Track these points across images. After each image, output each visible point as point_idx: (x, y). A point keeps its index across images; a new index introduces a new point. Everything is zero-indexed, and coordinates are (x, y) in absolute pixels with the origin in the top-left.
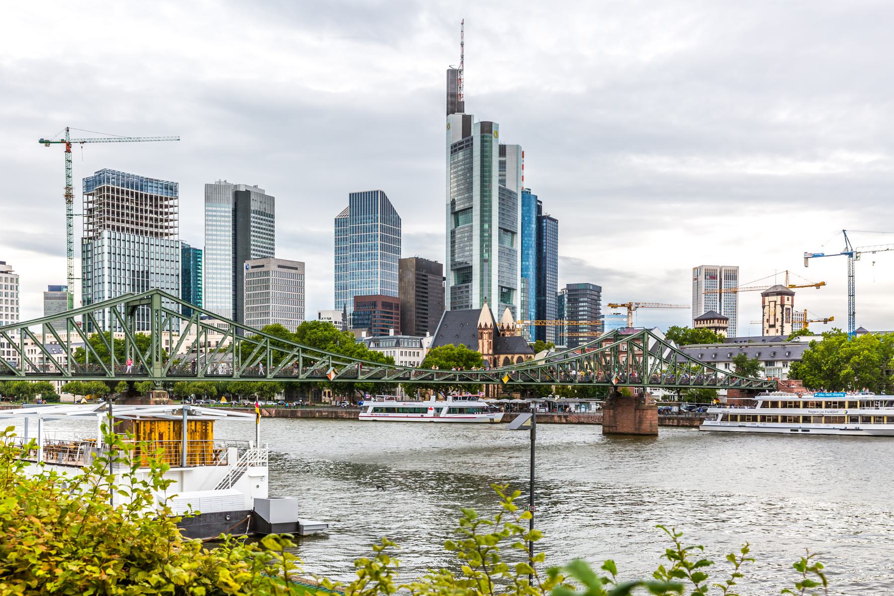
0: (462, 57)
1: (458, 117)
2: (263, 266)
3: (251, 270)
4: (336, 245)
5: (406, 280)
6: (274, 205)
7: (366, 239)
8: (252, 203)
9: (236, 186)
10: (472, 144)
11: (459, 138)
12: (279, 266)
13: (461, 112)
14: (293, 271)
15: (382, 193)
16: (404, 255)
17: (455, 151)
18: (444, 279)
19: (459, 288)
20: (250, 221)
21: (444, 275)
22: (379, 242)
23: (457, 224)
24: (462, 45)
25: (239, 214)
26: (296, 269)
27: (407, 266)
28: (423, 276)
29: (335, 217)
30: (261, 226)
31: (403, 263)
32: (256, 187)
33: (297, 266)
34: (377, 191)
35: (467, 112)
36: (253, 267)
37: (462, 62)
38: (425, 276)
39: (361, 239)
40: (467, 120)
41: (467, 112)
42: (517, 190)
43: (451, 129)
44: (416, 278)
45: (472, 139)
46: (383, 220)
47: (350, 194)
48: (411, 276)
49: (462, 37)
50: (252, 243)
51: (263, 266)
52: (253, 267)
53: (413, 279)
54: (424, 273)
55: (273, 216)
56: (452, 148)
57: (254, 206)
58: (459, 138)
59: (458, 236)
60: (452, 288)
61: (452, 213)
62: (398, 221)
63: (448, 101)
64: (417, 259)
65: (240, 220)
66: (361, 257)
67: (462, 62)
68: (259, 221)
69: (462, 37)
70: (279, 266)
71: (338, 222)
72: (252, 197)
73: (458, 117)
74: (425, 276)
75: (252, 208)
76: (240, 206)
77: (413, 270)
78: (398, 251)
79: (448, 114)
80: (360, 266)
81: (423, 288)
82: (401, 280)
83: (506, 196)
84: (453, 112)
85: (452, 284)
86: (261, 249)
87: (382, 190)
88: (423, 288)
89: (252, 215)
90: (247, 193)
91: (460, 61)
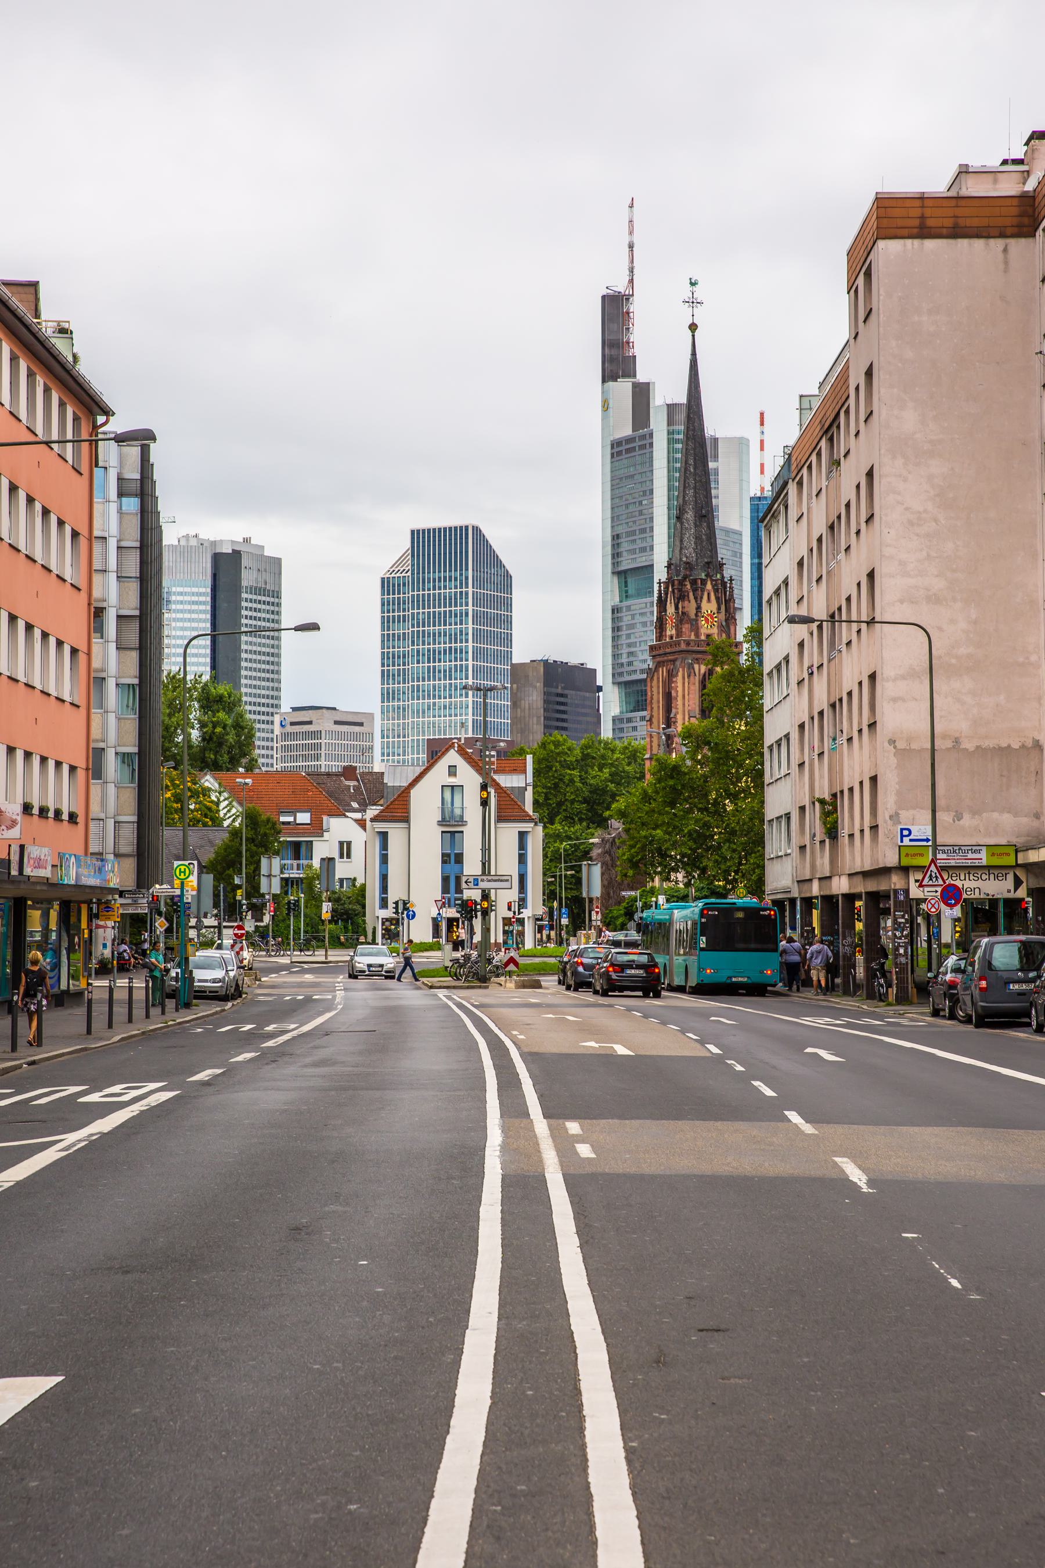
0: (631, 270)
1: (623, 388)
2: (310, 723)
3: (290, 729)
4: (383, 630)
5: (525, 704)
6: (280, 573)
7: (442, 618)
8: (244, 574)
9: (214, 543)
10: (651, 445)
11: (627, 431)
12: (336, 723)
13: (629, 376)
14: (357, 729)
15: (477, 530)
16: (521, 654)
17: (619, 453)
18: (600, 689)
19: (629, 720)
20: (239, 608)
21: (599, 682)
22: (470, 626)
23: (625, 595)
24: (631, 246)
25: (221, 595)
26: (361, 724)
27: (527, 676)
28: (558, 695)
29: (382, 573)
30: (259, 615)
31: (518, 672)
32: (247, 540)
33: (363, 720)
34: (467, 527)
35: (641, 377)
36: (292, 724)
37: (631, 281)
38: (562, 695)
39: (434, 619)
40: (642, 394)
41: (641, 377)
42: (741, 525)
43: (611, 411)
44: (546, 702)
45: (651, 435)
46: (479, 582)
47: (413, 532)
48: (535, 698)
49: (631, 233)
50: (244, 647)
51: (310, 723)
52: (292, 724)
53: (540, 704)
54: (559, 691)
55: (277, 594)
56: (612, 447)
57: (248, 578)
58: (627, 431)
59: (626, 619)
60: (615, 720)
61: (613, 573)
62: (506, 581)
63: (603, 356)
64: (546, 662)
65: (223, 605)
66: (433, 656)
67: (631, 281)
68: (254, 605)
69: (631, 233)
70: (336, 723)
71: (387, 584)
72: (245, 562)
73: (623, 388)
74: (562, 695)
75: (244, 583)
76: (222, 580)
77: (540, 685)
78: (509, 655)
79: (604, 381)
80: (432, 673)
81: (558, 720)
82: (515, 704)
83: (674, 661)
84: (614, 378)
85: (616, 711)
86: (254, 657)
87: (476, 523)
88: (558, 720)
89: (244, 595)
90: (236, 554)
91: (627, 278)
